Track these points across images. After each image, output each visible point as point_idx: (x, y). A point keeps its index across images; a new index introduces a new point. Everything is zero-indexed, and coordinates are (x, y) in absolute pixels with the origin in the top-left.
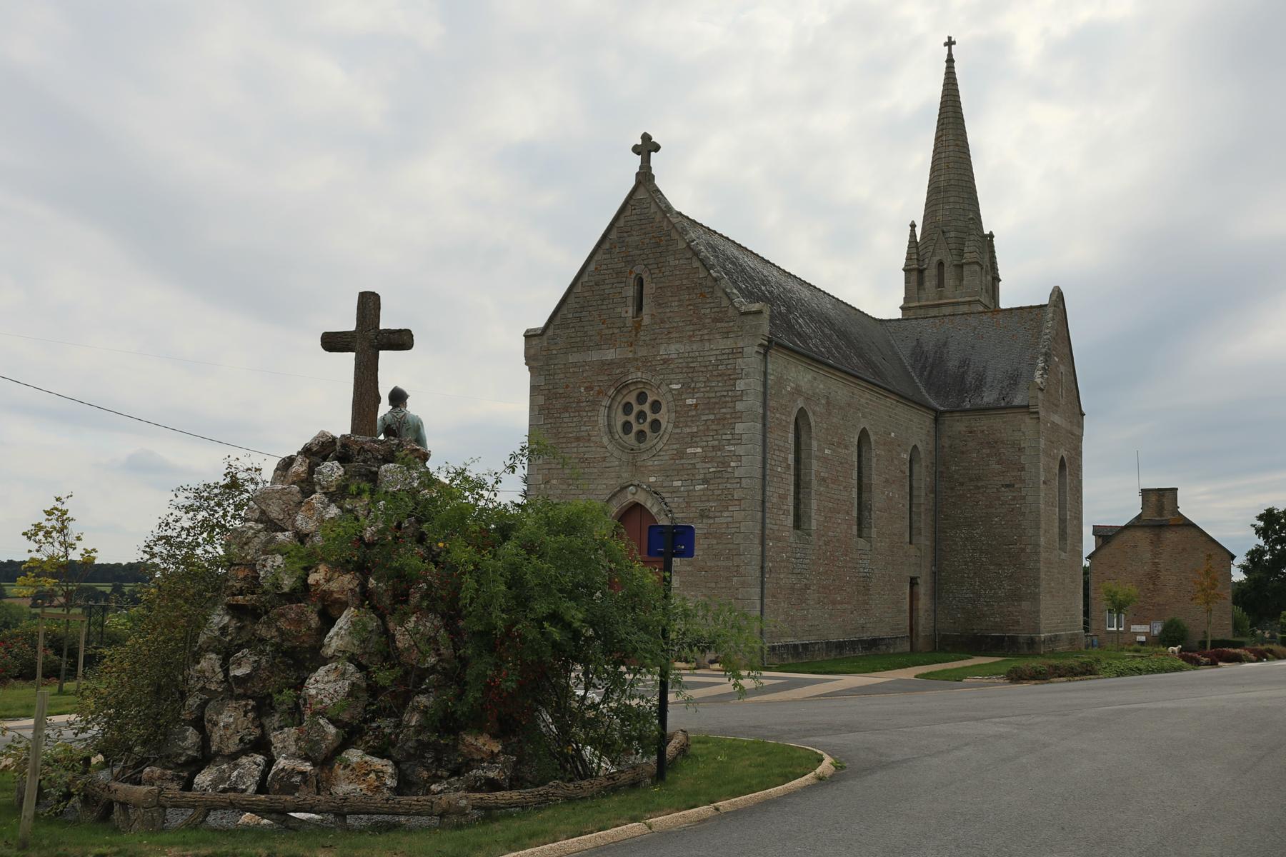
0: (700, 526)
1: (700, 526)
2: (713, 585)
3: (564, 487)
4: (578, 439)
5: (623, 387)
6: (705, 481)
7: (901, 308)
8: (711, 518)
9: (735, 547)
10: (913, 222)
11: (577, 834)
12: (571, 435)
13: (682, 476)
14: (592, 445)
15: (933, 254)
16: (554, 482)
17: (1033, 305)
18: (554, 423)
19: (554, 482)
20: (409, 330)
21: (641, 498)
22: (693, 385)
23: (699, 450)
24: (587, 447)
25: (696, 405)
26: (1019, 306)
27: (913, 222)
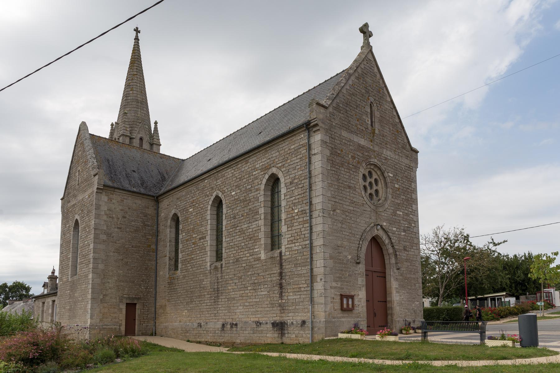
0: (404, 255)
1: (404, 255)
2: (410, 287)
3: (344, 216)
4: (350, 187)
5: (374, 164)
6: (404, 231)
7: (161, 145)
8: (407, 251)
9: (416, 268)
10: (156, 121)
11: (150, 332)
12: (345, 183)
13: (396, 225)
14: (357, 194)
15: (139, 133)
16: (338, 211)
17: (175, 157)
18: (336, 172)
19: (338, 211)
20: (372, 47)
21: (381, 233)
22: (397, 178)
23: (401, 213)
24: (354, 194)
25: (399, 189)
26: (168, 155)
27: (156, 121)
